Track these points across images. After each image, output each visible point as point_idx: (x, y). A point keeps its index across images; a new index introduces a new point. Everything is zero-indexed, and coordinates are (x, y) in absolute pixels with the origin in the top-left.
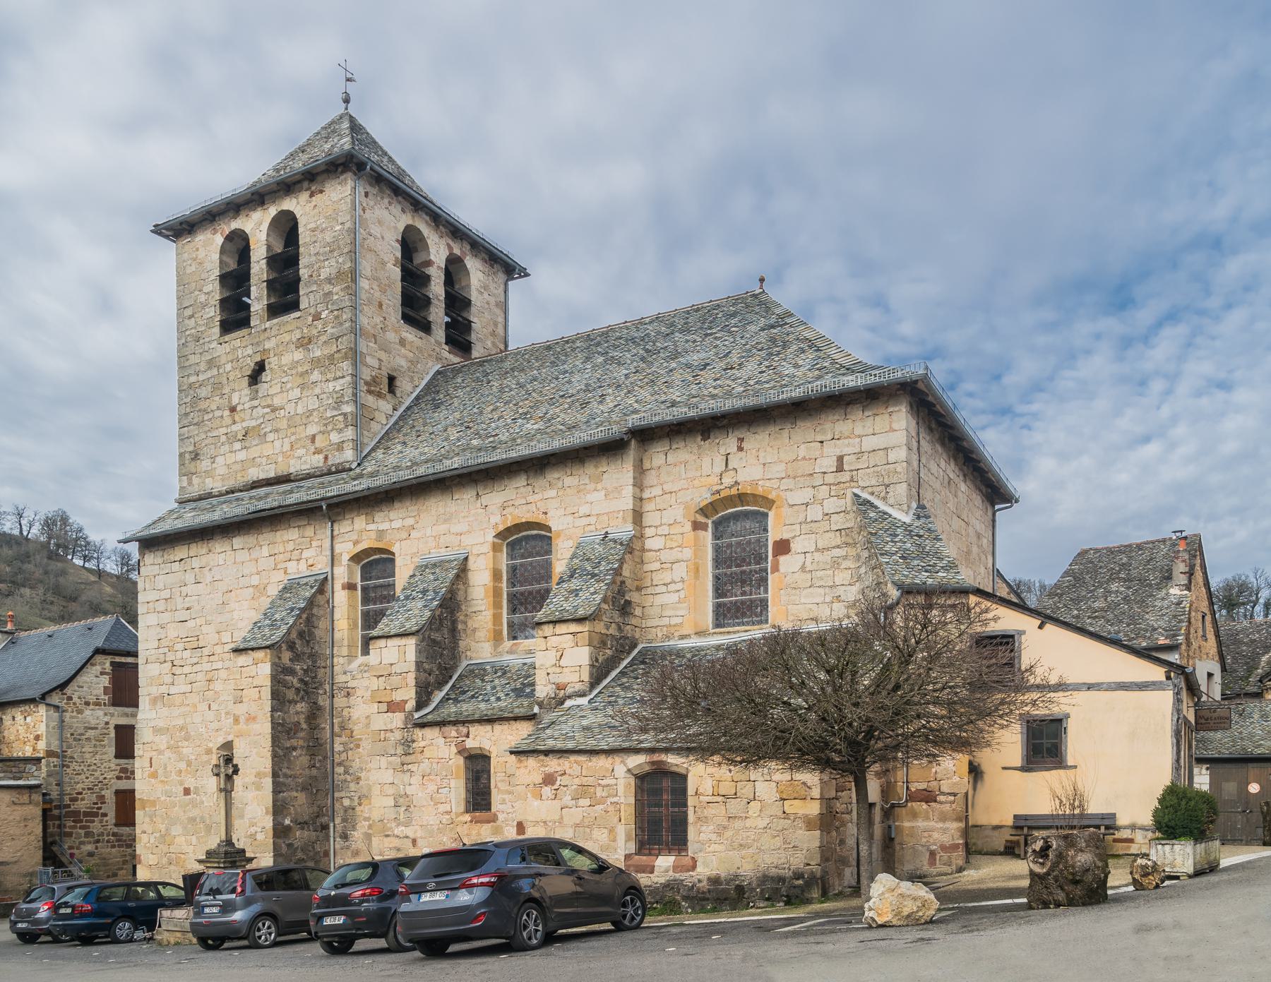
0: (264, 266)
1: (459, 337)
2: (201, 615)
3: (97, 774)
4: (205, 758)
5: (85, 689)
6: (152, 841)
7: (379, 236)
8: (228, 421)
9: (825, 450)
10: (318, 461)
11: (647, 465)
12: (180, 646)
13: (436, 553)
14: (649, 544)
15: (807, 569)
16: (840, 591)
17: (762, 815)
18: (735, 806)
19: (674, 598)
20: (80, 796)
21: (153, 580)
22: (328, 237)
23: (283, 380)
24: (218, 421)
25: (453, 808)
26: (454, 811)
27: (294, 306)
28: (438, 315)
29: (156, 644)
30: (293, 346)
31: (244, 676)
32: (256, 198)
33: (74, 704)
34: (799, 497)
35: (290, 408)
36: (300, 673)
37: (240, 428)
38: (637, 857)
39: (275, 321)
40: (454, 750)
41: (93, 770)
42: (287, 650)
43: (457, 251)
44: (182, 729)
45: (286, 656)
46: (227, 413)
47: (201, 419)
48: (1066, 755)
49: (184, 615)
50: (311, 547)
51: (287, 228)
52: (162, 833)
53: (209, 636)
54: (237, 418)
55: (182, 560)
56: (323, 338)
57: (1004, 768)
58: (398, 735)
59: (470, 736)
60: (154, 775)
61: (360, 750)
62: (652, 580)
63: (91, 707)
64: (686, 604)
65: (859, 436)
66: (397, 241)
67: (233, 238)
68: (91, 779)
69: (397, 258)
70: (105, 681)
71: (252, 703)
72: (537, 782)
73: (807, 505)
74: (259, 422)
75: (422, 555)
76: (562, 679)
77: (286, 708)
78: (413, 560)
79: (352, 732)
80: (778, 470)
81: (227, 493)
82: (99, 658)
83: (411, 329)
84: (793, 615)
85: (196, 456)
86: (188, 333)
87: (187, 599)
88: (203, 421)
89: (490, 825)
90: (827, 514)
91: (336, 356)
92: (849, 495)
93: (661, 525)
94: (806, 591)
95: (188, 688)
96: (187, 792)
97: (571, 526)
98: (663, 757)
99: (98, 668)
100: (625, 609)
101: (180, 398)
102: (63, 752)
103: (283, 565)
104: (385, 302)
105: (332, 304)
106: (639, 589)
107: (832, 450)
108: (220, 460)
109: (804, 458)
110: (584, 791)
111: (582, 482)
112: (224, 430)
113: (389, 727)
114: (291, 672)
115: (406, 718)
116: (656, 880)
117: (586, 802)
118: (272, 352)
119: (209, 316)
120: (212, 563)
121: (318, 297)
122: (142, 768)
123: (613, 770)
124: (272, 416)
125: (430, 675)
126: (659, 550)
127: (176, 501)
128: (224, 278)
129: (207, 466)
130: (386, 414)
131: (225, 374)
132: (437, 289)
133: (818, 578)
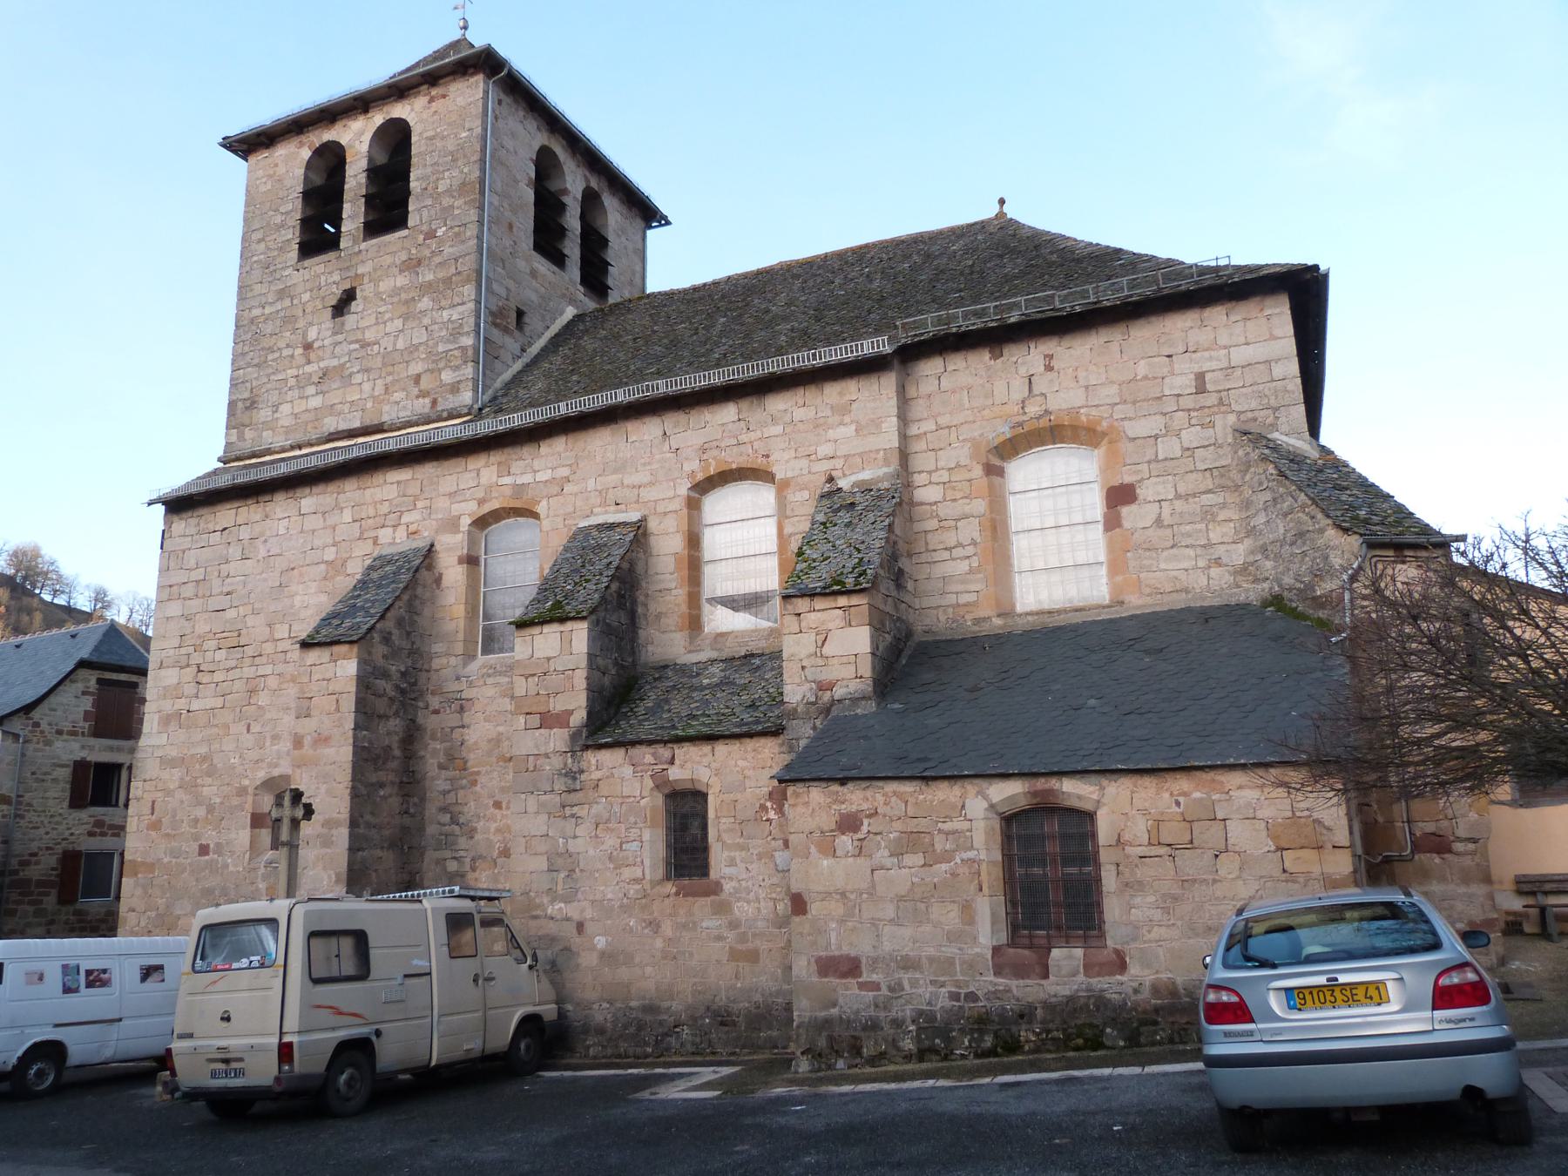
0: (364, 181)
1: (595, 276)
2: (246, 601)
3: (61, 828)
4: (235, 801)
5: (59, 713)
6: (143, 924)
7: (512, 149)
8: (300, 360)
9: (1176, 366)
10: (422, 406)
11: (911, 392)
12: (212, 644)
14: (922, 494)
15: (1166, 523)
16: (1220, 551)
17: (1245, 876)
18: (1191, 863)
19: (963, 567)
20: (34, 859)
21: (181, 555)
22: (451, 145)
23: (379, 310)
24: (286, 362)
25: (647, 872)
26: (648, 877)
28: (572, 249)
29: (176, 642)
30: (396, 271)
31: (315, 677)
32: (360, 104)
33: (42, 732)
35: (387, 343)
36: (396, 676)
38: (1011, 951)
39: (374, 241)
40: (649, 783)
41: (57, 823)
43: (594, 184)
44: (204, 759)
45: (380, 650)
46: (299, 351)
47: (263, 359)
49: (223, 602)
50: (415, 508)
51: (396, 138)
52: (161, 910)
53: (256, 628)
55: (225, 529)
56: (437, 260)
58: (557, 762)
59: (677, 762)
60: (155, 826)
61: (478, 788)
62: (927, 544)
63: (65, 737)
64: (982, 575)
66: (532, 160)
68: (53, 834)
70: (87, 703)
72: (826, 828)
73: (1156, 437)
74: (342, 361)
76: (827, 675)
78: (567, 522)
79: (466, 762)
80: (1110, 393)
82: (83, 673)
83: (543, 260)
85: (252, 404)
86: (255, 258)
87: (229, 580)
88: (265, 362)
89: (709, 899)
90: (1188, 449)
91: (454, 278)
93: (937, 469)
94: (1165, 553)
95: (219, 702)
96: (204, 850)
97: (805, 472)
98: (1054, 783)
99: (80, 686)
100: (899, 578)
101: (236, 335)
102: (18, 796)
103: (372, 534)
104: (516, 224)
105: (453, 219)
106: (910, 555)
108: (285, 409)
109: (1146, 378)
110: (911, 842)
111: (819, 415)
112: (294, 372)
113: (542, 751)
114: (385, 675)
117: (918, 859)
118: (366, 280)
119: (284, 239)
120: (268, 533)
121: (433, 212)
123: (963, 806)
124: (362, 353)
125: (604, 674)
126: (936, 503)
127: (219, 460)
129: (267, 416)
130: (512, 354)
131: (300, 306)
132: (572, 221)
133: (1183, 535)
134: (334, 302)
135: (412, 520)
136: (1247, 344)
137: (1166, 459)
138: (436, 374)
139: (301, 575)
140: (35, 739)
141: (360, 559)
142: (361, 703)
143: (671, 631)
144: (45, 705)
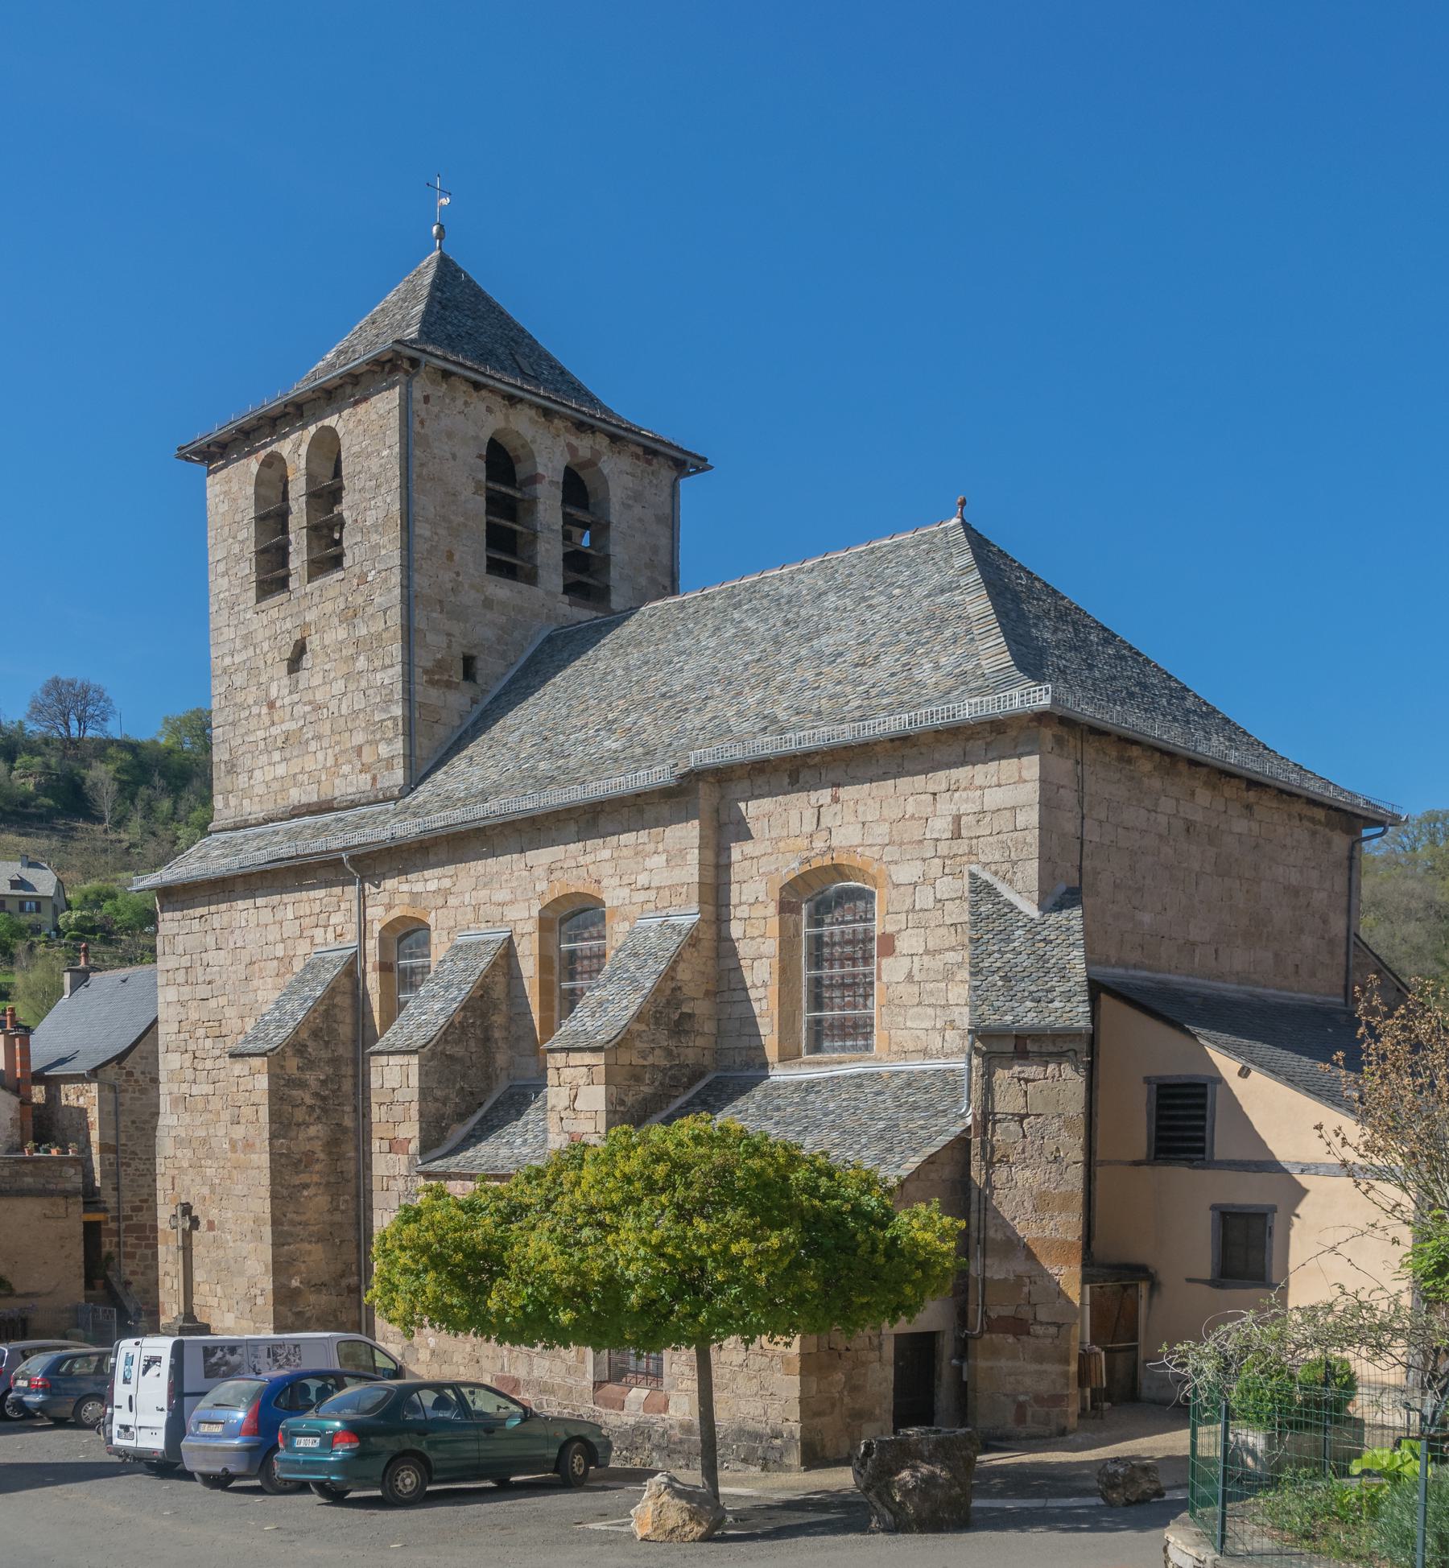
8: (266, 720)
12: (201, 1032)
13: (475, 928)
15: (916, 979)
20: (145, 1205)
27: (336, 562)
28: (549, 552)
30: (335, 620)
31: (241, 1088)
34: (905, 873)
37: (279, 731)
39: (316, 584)
42: (294, 1055)
45: (292, 1064)
46: (265, 710)
48: (1271, 1265)
49: (203, 991)
50: (339, 910)
51: (328, 449)
54: (276, 718)
57: (1190, 1280)
65: (981, 788)
66: (480, 456)
67: (272, 464)
69: (478, 482)
71: (249, 1125)
73: (915, 885)
75: (459, 931)
77: (293, 1134)
81: (266, 821)
84: (896, 1043)
86: (222, 596)
90: (940, 901)
92: (966, 874)
97: (627, 902)
107: (947, 807)
108: (257, 774)
112: (261, 734)
114: (302, 1084)
115: (410, 1163)
116: (625, 1419)
118: (313, 627)
122: (165, 1190)
128: (260, 519)
131: (262, 656)
134: (288, 655)
135: (338, 922)
136: (999, 786)
137: (921, 910)
138: (374, 746)
139: (261, 970)
140: (130, 1089)
141: (301, 958)
142: (275, 1117)
143: (953, 900)
144: (135, 1054)
